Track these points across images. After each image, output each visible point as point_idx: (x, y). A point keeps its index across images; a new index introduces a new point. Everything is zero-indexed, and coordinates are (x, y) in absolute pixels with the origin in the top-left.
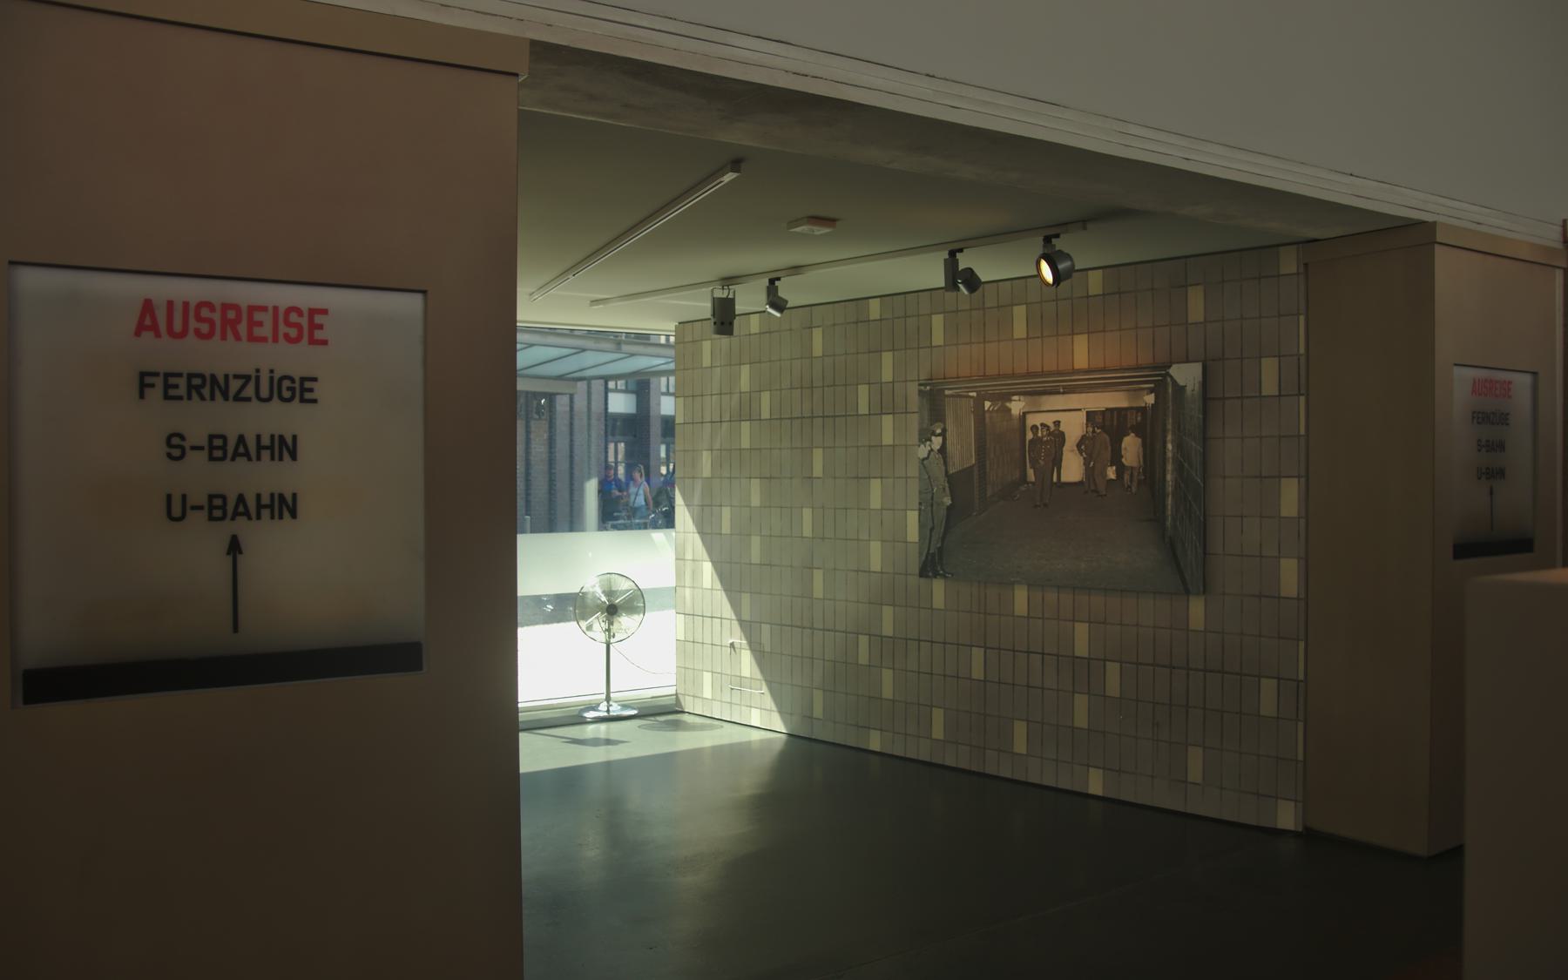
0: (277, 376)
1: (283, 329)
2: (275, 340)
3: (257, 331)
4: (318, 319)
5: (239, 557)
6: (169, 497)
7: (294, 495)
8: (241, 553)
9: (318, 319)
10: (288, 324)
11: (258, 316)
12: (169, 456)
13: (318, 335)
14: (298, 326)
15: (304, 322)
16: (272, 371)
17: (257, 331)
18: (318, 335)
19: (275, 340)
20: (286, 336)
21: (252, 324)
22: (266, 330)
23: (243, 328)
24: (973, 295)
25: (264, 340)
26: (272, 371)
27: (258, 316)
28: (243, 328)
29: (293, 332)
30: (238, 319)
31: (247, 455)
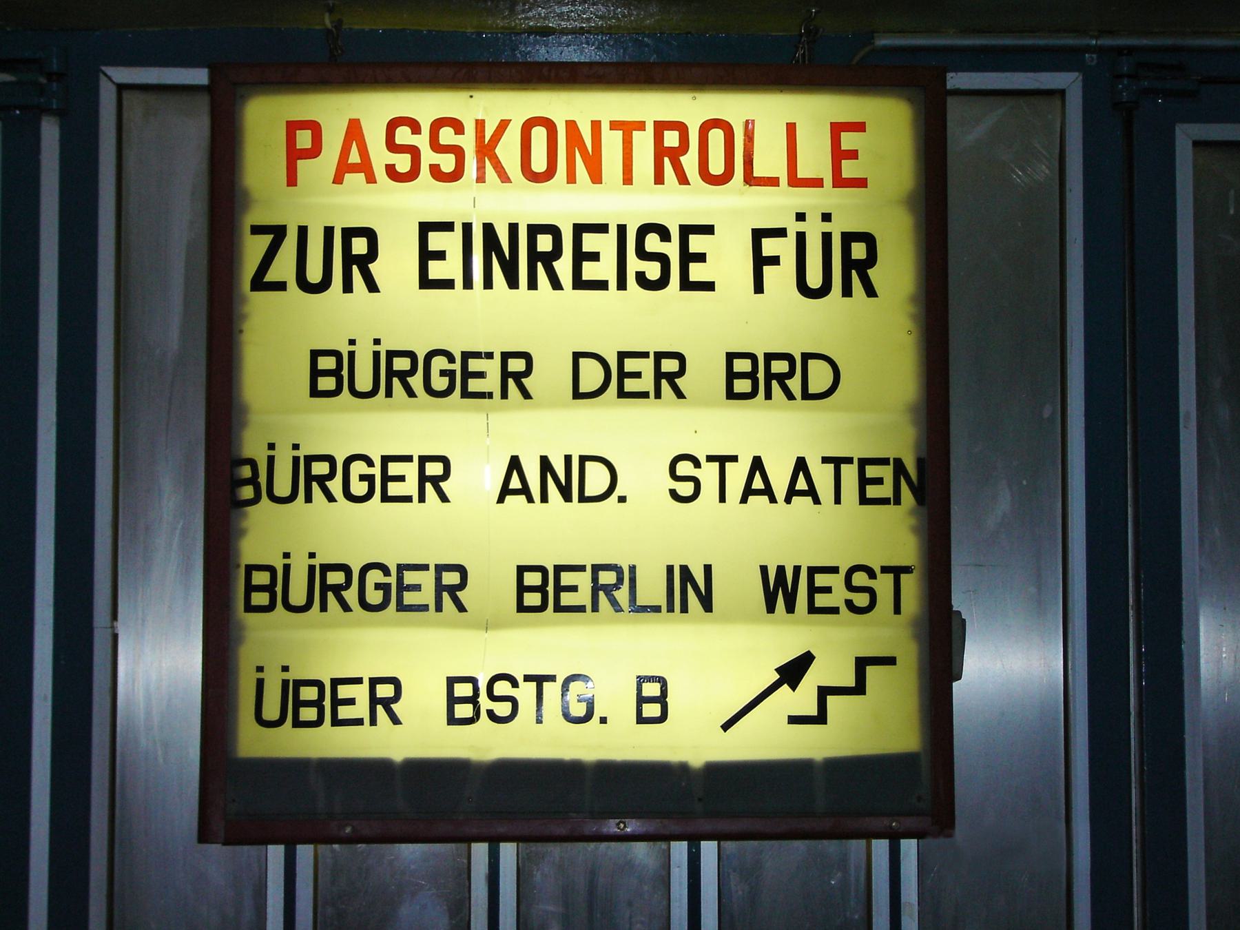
0: (383, 349)
1: (634, 264)
2: (622, 285)
3: (590, 271)
4: (697, 243)
5: (785, 688)
6: (670, 569)
7: (708, 569)
8: (794, 688)
9: (697, 243)
10: (642, 254)
11: (590, 242)
12: (674, 494)
13: (697, 272)
14: (663, 259)
15: (672, 249)
16: (377, 342)
17: (590, 271)
18: (697, 272)
19: (622, 285)
20: (641, 279)
21: (580, 257)
22: (604, 269)
23: (564, 267)
24: (1191, 142)
25: (448, 284)
26: (377, 342)
27: (590, 242)
28: (564, 267)
29: (653, 271)
30: (557, 252)
31: (525, 491)
